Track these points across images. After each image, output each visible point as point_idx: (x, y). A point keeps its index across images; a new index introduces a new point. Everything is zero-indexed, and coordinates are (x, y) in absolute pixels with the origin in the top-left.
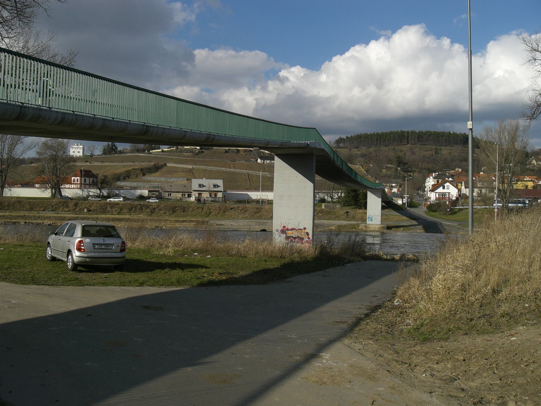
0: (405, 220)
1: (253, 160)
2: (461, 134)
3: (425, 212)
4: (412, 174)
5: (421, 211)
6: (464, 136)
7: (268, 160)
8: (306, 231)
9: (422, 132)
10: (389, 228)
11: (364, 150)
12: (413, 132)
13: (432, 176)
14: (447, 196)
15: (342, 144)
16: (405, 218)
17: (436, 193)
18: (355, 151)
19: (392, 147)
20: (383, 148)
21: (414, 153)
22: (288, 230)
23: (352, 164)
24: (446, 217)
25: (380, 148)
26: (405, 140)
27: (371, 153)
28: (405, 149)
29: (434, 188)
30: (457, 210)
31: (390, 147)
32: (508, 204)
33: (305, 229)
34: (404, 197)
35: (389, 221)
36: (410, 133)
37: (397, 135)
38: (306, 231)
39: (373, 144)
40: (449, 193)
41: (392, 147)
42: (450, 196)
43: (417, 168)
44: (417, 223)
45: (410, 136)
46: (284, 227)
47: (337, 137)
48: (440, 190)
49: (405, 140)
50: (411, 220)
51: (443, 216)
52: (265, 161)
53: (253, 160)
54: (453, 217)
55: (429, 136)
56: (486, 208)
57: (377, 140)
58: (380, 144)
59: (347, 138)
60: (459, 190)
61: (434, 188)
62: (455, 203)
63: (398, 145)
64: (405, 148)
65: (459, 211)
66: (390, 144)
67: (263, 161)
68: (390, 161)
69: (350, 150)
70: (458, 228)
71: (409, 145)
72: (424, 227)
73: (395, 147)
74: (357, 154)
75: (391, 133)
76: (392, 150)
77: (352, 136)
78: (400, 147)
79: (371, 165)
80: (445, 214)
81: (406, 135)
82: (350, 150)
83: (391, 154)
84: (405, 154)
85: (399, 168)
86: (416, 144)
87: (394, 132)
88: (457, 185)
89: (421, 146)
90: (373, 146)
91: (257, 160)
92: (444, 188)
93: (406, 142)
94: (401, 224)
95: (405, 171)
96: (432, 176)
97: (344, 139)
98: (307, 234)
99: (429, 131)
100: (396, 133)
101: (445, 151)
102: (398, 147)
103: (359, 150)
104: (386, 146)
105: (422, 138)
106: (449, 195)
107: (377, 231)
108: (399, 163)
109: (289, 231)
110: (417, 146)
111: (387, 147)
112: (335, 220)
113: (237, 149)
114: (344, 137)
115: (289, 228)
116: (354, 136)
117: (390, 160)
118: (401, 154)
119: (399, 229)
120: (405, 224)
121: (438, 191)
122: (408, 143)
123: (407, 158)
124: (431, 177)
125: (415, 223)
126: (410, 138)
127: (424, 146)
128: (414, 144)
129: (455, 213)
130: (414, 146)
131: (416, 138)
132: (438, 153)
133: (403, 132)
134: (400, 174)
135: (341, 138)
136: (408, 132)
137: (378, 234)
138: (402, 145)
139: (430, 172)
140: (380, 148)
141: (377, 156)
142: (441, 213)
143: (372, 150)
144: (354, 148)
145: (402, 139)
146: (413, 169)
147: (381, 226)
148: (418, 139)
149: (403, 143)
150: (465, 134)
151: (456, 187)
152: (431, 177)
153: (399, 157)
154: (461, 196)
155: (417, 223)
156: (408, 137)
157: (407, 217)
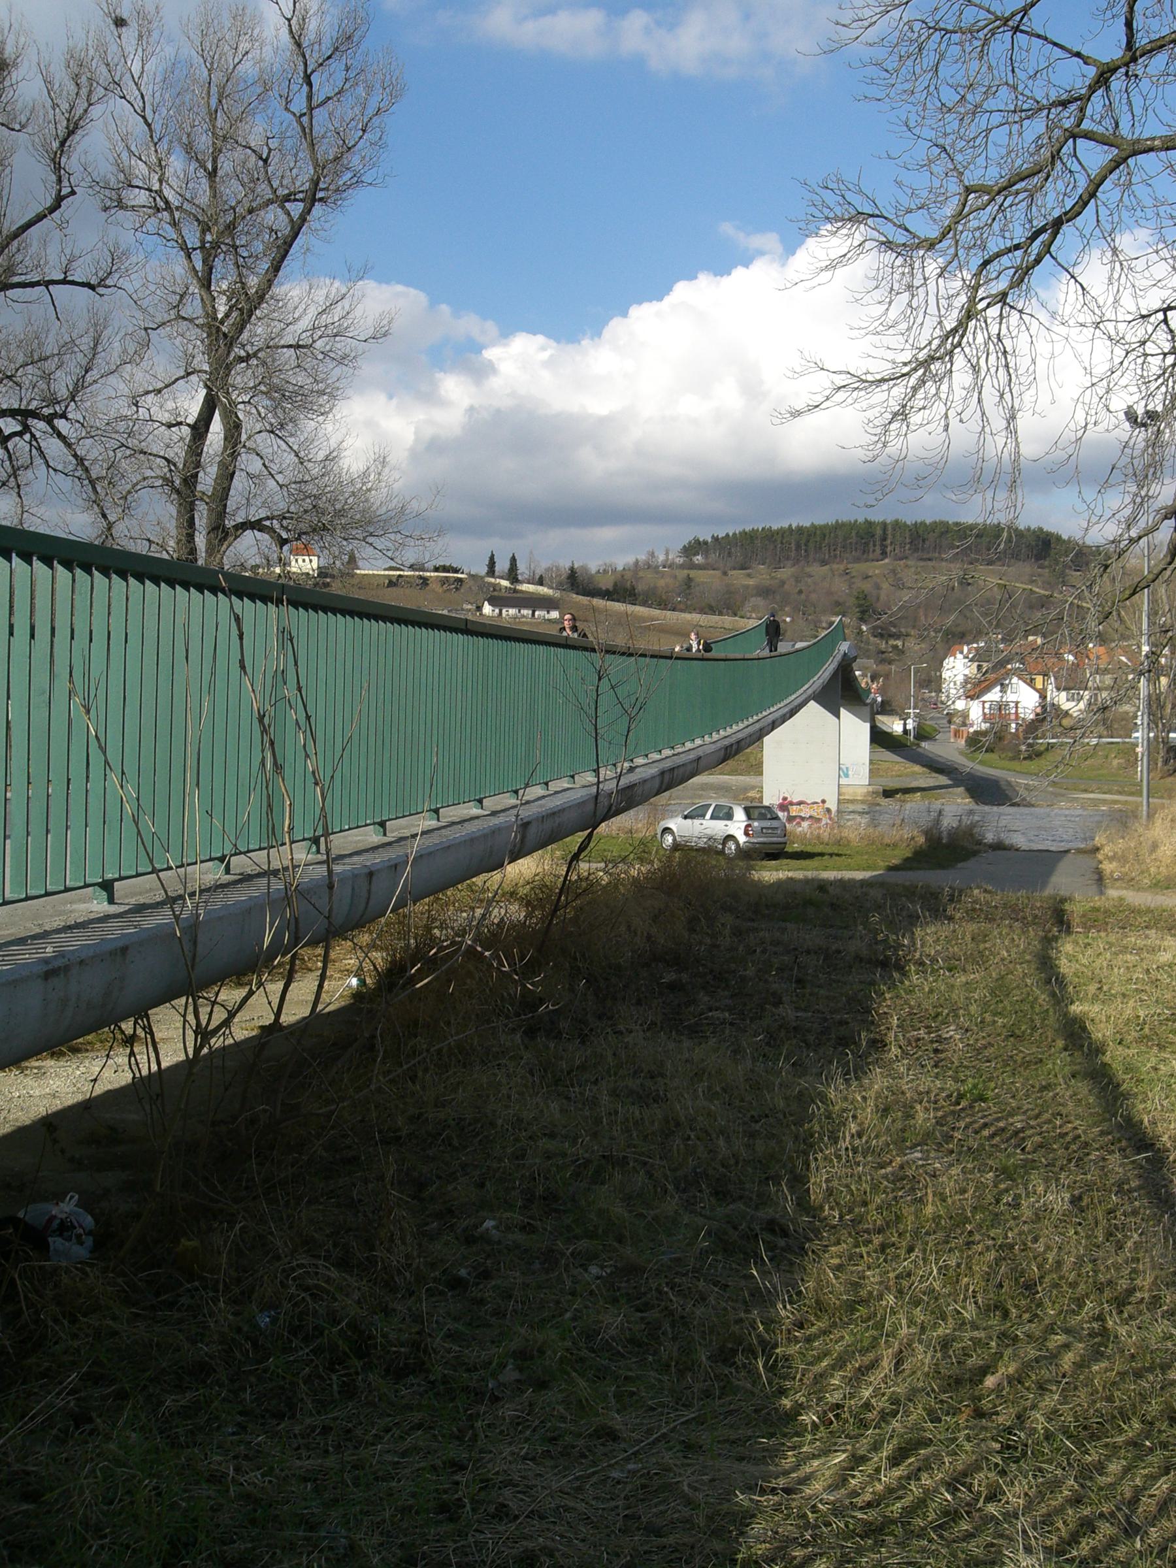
0: (920, 777)
1: (469, 607)
2: (1029, 529)
3: (961, 753)
4: (899, 643)
5: (949, 748)
6: (1038, 537)
7: (513, 607)
8: (826, 805)
9: (923, 523)
10: (888, 793)
11: (761, 574)
12: (897, 524)
13: (962, 652)
14: (1013, 711)
15: (699, 557)
16: (917, 768)
17: (984, 702)
18: (739, 579)
19: (842, 567)
20: (817, 570)
21: (899, 585)
22: (792, 804)
23: (735, 615)
24: (1015, 765)
25: (808, 570)
26: (874, 545)
27: (783, 583)
28: (877, 572)
29: (975, 689)
30: (1042, 749)
31: (835, 566)
32: (1169, 732)
33: (824, 802)
34: (908, 716)
35: (882, 776)
36: (890, 528)
37: (854, 534)
38: (826, 805)
39: (788, 559)
40: (1017, 703)
41: (842, 567)
42: (1020, 710)
43: (914, 627)
44: (950, 782)
45: (890, 536)
46: (785, 799)
47: (686, 535)
48: (994, 695)
49: (874, 545)
50: (934, 775)
51: (1007, 764)
52: (504, 611)
53: (469, 607)
54: (1032, 765)
55: (942, 534)
56: (1112, 743)
57: (798, 547)
58: (807, 556)
59: (716, 539)
60: (1043, 697)
61: (975, 689)
62: (1033, 727)
63: (857, 560)
64: (877, 568)
65: (1047, 749)
66: (835, 556)
67: (497, 611)
68: (838, 607)
69: (725, 573)
70: (1052, 793)
71: (886, 561)
72: (968, 790)
73: (849, 566)
74: (747, 587)
75: (838, 526)
76: (840, 575)
77: (727, 535)
78: (858, 568)
79: (788, 619)
80: (1013, 759)
81: (879, 532)
82: (725, 573)
83: (840, 587)
84: (878, 587)
85: (864, 628)
86: (906, 558)
87: (843, 524)
88: (1032, 680)
89: (922, 563)
90: (789, 563)
91: (479, 608)
92: (1003, 690)
93: (878, 551)
94: (914, 784)
95: (881, 636)
96: (962, 652)
97: (706, 543)
98: (828, 810)
99: (942, 522)
100: (853, 526)
101: (989, 579)
102: (856, 565)
103: (749, 575)
104: (824, 563)
105: (924, 541)
106: (1017, 707)
107: (863, 802)
108: (863, 612)
109: (794, 807)
110: (909, 563)
111: (827, 567)
112: (748, 774)
113: (420, 577)
114: (706, 536)
115: (795, 801)
116: (734, 534)
117: (838, 604)
118: (867, 586)
119: (911, 795)
120: (922, 783)
121: (987, 697)
122: (884, 554)
123: (883, 597)
124: (959, 656)
125: (943, 780)
126: (889, 541)
127: (930, 563)
128: (901, 559)
129: (1039, 754)
130: (902, 562)
131: (908, 540)
132: (969, 584)
133: (869, 524)
134: (868, 643)
135: (697, 542)
136: (884, 525)
137: (859, 807)
138: (867, 561)
139: (954, 638)
140: (808, 570)
141: (800, 592)
142: (1003, 756)
143: (786, 573)
144: (735, 569)
145: (866, 544)
146: (903, 630)
147: (870, 789)
148: (911, 543)
149: (871, 556)
150: (1041, 529)
151: (1031, 683)
152: (959, 656)
153: (863, 597)
154: (1047, 713)
155: (950, 782)
156: (885, 539)
157: (923, 766)
